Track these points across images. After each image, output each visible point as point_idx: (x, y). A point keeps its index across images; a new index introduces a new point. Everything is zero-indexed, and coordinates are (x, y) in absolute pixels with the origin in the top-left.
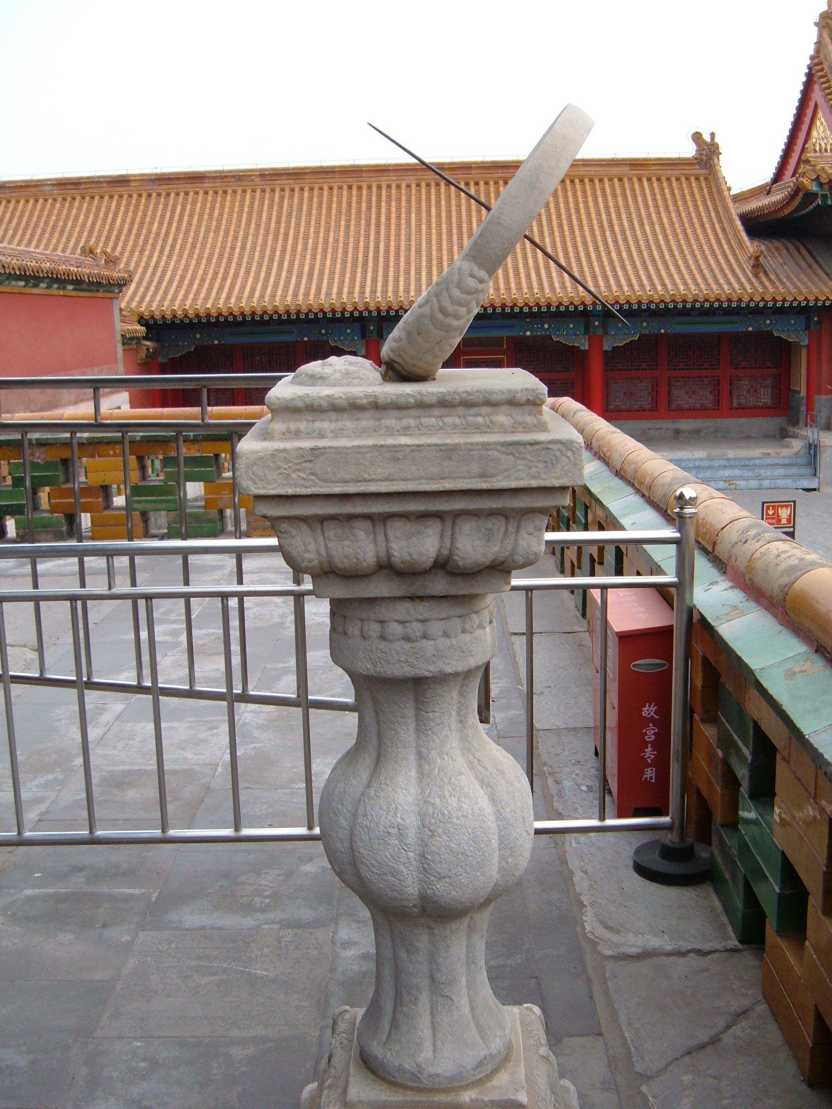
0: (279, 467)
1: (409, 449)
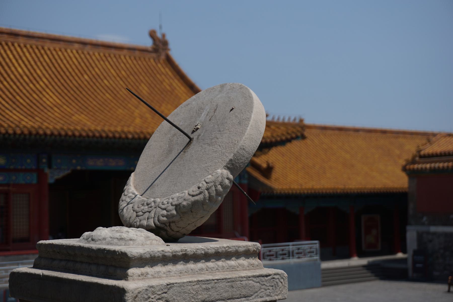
0: (149, 298)
1: (213, 282)
